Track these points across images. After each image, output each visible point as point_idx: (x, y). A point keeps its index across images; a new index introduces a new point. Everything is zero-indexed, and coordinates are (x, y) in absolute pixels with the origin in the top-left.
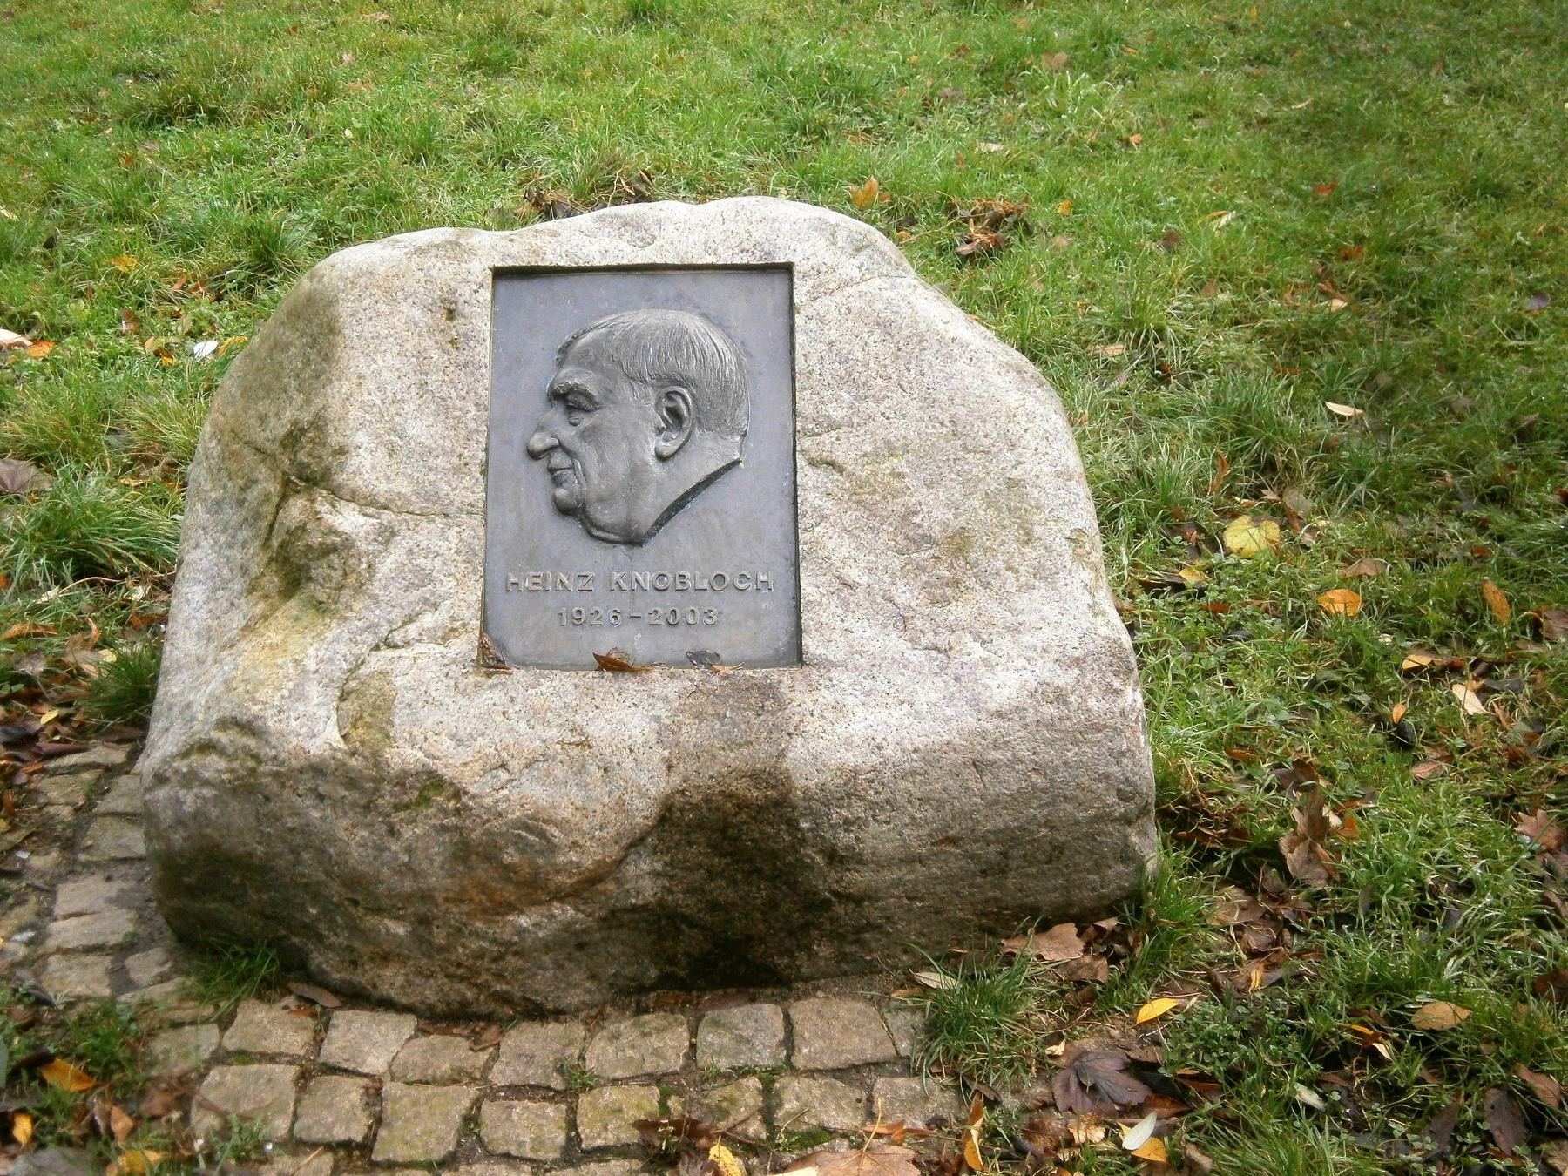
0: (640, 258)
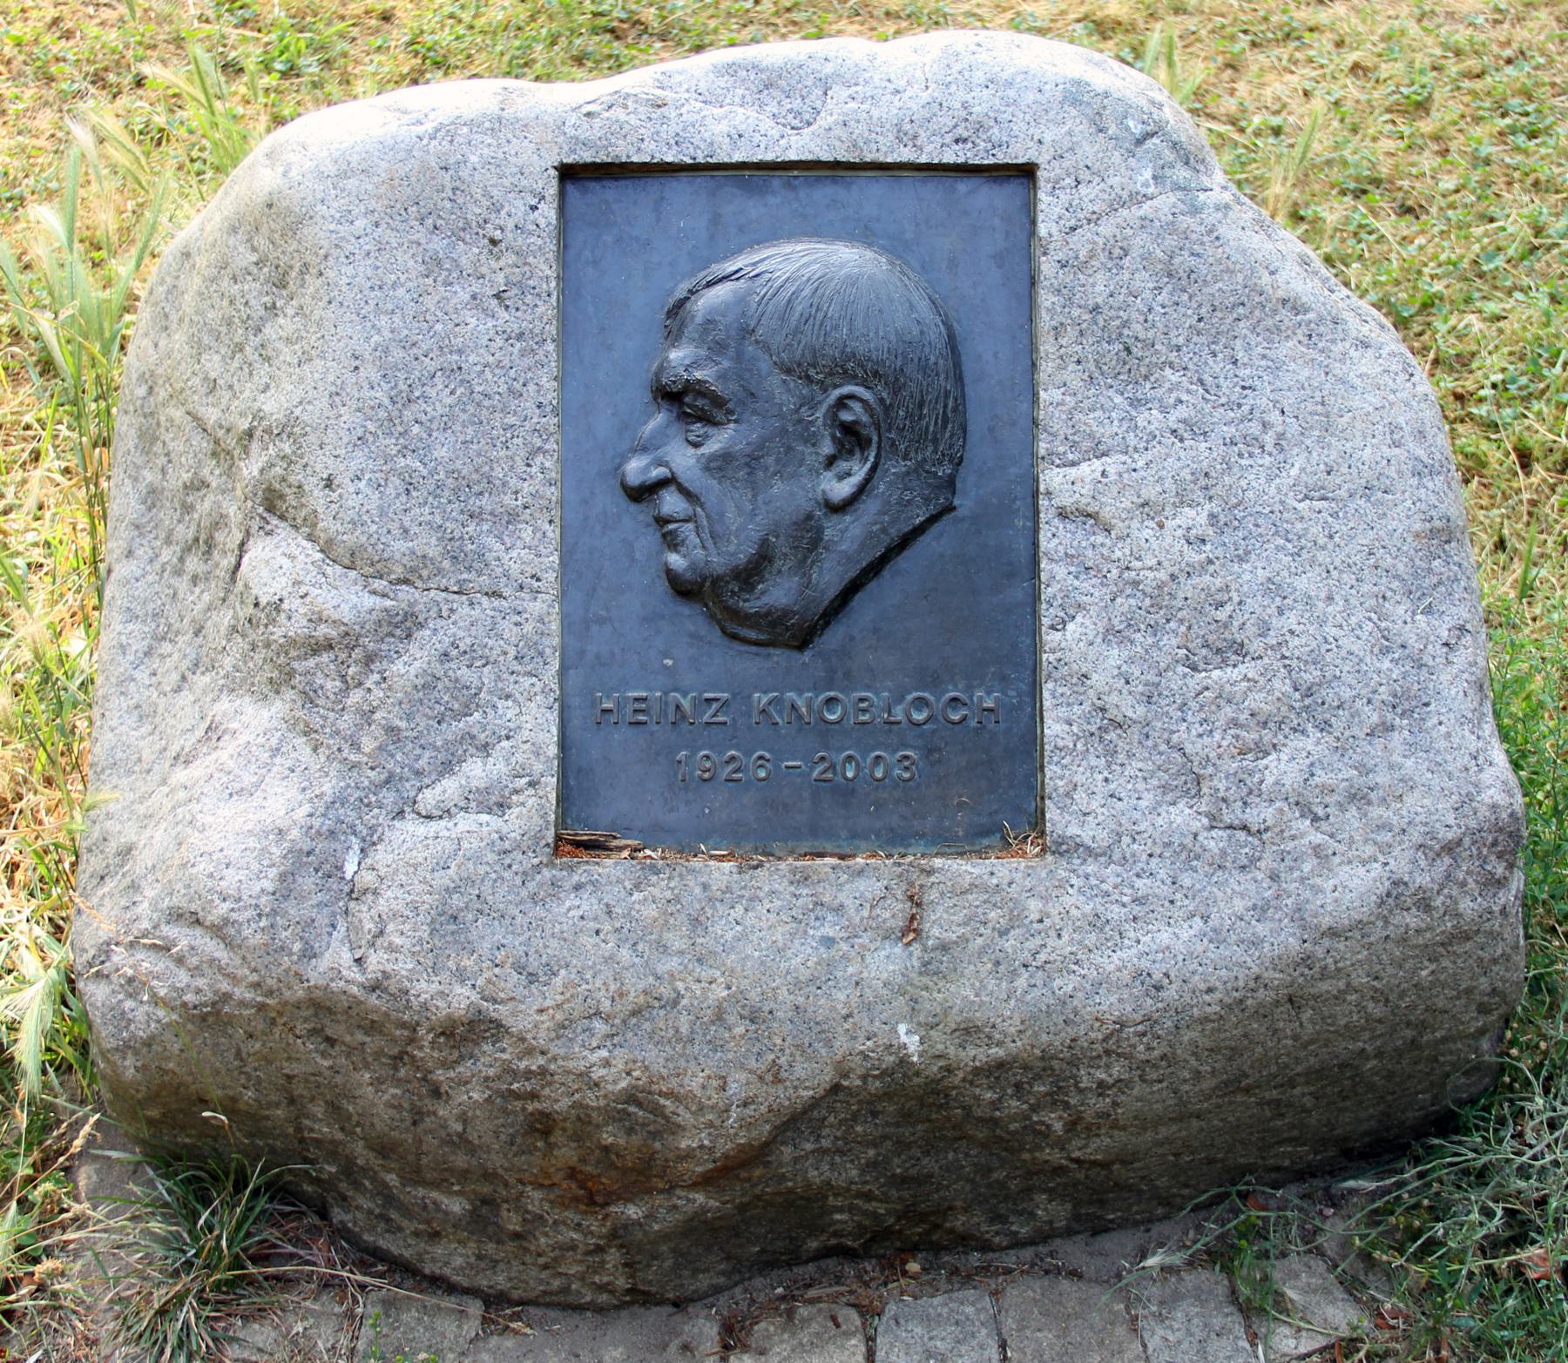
0: (798, 147)
